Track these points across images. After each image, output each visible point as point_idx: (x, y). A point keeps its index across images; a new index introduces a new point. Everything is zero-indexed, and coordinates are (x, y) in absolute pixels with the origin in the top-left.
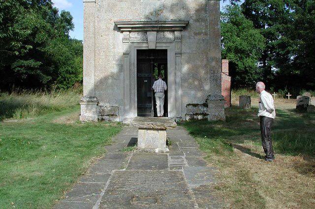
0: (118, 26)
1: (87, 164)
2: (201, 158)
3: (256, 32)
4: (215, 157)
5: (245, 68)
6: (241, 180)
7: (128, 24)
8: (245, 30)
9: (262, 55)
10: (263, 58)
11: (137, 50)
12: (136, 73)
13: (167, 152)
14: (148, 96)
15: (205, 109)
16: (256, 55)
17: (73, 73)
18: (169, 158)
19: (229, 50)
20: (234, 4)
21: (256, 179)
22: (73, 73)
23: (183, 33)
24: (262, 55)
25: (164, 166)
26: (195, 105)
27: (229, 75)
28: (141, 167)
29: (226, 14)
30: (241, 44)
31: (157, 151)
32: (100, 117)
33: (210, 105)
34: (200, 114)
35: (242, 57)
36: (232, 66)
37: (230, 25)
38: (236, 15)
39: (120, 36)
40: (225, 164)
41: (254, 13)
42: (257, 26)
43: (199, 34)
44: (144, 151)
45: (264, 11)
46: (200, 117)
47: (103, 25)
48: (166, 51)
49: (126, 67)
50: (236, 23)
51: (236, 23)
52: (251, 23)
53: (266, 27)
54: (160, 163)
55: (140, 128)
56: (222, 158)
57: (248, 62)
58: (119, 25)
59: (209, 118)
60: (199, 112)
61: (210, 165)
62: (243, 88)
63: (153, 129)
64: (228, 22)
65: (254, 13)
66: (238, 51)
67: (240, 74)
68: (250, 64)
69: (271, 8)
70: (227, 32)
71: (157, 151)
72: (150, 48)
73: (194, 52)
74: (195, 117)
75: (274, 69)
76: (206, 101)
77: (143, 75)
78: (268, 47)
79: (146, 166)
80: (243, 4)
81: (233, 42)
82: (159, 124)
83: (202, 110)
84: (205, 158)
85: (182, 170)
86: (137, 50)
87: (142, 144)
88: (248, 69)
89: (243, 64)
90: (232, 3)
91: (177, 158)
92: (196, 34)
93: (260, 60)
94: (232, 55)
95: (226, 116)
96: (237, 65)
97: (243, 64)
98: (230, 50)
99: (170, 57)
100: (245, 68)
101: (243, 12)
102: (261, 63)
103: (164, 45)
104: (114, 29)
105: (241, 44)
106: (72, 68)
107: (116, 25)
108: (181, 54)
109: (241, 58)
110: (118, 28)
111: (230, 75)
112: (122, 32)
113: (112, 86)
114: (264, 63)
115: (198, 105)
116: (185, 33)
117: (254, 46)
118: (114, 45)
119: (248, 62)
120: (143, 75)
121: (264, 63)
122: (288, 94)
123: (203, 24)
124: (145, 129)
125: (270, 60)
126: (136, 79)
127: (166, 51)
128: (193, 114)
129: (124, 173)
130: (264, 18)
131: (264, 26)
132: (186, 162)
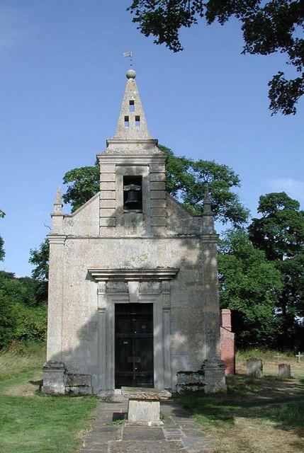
0: (93, 274)
1: (80, 434)
2: (199, 430)
3: (268, 266)
4: (214, 429)
5: (256, 318)
6: (240, 447)
7: (105, 272)
8: (255, 263)
9: (280, 300)
10: (282, 303)
11: (116, 304)
12: (114, 333)
13: (161, 425)
14: (129, 361)
15: (201, 377)
16: (270, 299)
17: (9, 326)
18: (164, 431)
19: (232, 293)
20: (239, 227)
21: (255, 445)
22: (9, 326)
23: (171, 283)
24: (280, 300)
25: (161, 437)
26: (188, 373)
27: (232, 331)
28: (138, 438)
29: (226, 242)
30: (249, 285)
31: (150, 424)
32: (68, 389)
33: (207, 372)
34: (195, 384)
35: (250, 303)
36: (237, 318)
37: (234, 257)
38: (242, 242)
39: (95, 286)
40: (225, 435)
41: (266, 238)
42: (271, 256)
43: (192, 284)
44: (135, 424)
45: (281, 236)
46: (195, 388)
47: (72, 272)
48: (151, 305)
49: (102, 325)
50: (242, 255)
51: (242, 255)
52: (263, 253)
53: (285, 258)
54: (155, 434)
55: (130, 399)
56: (222, 430)
57: (261, 309)
58: (94, 272)
59: (206, 389)
60: (193, 382)
61: (209, 436)
62: (254, 346)
63: (145, 400)
64: (229, 253)
65: (266, 238)
66: (245, 294)
67: (250, 326)
68: (264, 312)
69: (290, 232)
70: (230, 268)
71: (150, 424)
72: (132, 302)
73: (186, 307)
74: (188, 388)
75: (298, 318)
76: (98, 163)
77: (122, 335)
78: (288, 286)
79: (140, 437)
80: (251, 226)
81: (238, 282)
82: (152, 394)
83: (197, 378)
84: (203, 430)
85: (181, 440)
86: (116, 304)
87: (133, 417)
88: (259, 319)
89: (253, 313)
90: (235, 226)
91: (173, 431)
92: (188, 284)
93: (277, 305)
94: (237, 302)
95: (228, 388)
96: (245, 315)
97: (253, 313)
98: (234, 294)
99: (157, 312)
100: (256, 318)
101: (251, 238)
102: (279, 310)
103: (150, 298)
104: (87, 278)
105: (249, 285)
106: (8, 318)
107: (89, 273)
108: (169, 309)
109: (250, 304)
110: (92, 277)
111: (233, 331)
112: (97, 281)
113: (83, 349)
114: (284, 310)
115: (192, 372)
116: (174, 283)
117: (268, 287)
118: (86, 297)
119: (261, 309)
120: (122, 335)
121: (284, 310)
122: (298, 354)
123: (196, 271)
124: (137, 399)
125: (292, 305)
126: (114, 340)
127: (151, 305)
128: (187, 385)
129: (122, 443)
130: (282, 246)
131: (281, 257)
132: (183, 433)
